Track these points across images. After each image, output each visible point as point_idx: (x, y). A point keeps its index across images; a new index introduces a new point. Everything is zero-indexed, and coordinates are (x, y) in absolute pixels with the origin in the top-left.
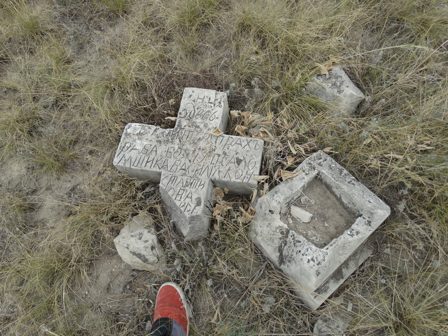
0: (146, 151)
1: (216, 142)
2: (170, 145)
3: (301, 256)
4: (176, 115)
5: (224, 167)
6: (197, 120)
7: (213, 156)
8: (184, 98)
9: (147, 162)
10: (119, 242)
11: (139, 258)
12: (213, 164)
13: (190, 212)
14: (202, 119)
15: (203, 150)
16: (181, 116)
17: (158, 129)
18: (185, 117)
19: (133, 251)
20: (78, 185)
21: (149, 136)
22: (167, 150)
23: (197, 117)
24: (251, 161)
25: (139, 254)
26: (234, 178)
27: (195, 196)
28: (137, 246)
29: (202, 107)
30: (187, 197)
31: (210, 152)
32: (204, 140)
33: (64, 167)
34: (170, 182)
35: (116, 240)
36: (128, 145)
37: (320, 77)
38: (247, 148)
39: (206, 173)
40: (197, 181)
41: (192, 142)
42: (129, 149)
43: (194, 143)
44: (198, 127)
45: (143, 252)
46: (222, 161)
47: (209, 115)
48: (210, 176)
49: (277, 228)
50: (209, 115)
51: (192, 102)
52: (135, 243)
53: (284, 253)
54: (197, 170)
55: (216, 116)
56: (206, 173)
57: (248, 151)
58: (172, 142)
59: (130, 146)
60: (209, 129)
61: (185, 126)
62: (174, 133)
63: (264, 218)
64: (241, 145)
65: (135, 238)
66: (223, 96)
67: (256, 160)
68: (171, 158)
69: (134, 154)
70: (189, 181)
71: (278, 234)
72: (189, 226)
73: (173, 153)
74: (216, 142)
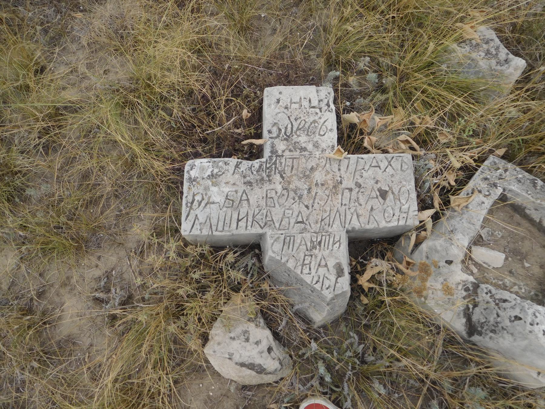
0: (231, 202)
1: (339, 170)
2: (267, 186)
3: (529, 327)
4: (259, 136)
5: (363, 207)
6: (300, 138)
7: (341, 192)
8: (269, 105)
9: (239, 220)
10: (214, 352)
11: (250, 369)
12: (345, 205)
13: (332, 289)
14: (307, 135)
15: (322, 185)
16: (271, 136)
17: (241, 163)
18: (278, 136)
19: (241, 361)
20: (112, 271)
21: (229, 177)
22: (265, 196)
23: (298, 133)
24: (402, 191)
25: (251, 364)
26: (384, 222)
27: (331, 263)
28: (248, 354)
29: (302, 116)
30: (319, 265)
31: (335, 187)
32: (320, 169)
33: (82, 245)
34: (286, 247)
35: (208, 350)
36: (198, 198)
37: (463, 45)
38: (389, 169)
39: (337, 222)
40: (328, 237)
41: (301, 175)
42: (203, 204)
43: (307, 177)
44: (304, 149)
45: (258, 361)
46: (358, 198)
47: (316, 127)
48: (346, 226)
49: (459, 284)
50: (316, 127)
51: (283, 110)
52: (239, 349)
53: (475, 318)
54: (322, 220)
55: (329, 128)
56: (337, 222)
57: (392, 176)
58: (270, 181)
59: (203, 199)
60: (323, 150)
61: (283, 151)
62: (268, 166)
63: (437, 272)
64: (379, 167)
65: (239, 341)
66: (326, 92)
67: (408, 188)
68: (274, 207)
69: (213, 210)
70: (314, 239)
71: (460, 292)
72: (328, 308)
73: (276, 198)
74: (339, 170)
